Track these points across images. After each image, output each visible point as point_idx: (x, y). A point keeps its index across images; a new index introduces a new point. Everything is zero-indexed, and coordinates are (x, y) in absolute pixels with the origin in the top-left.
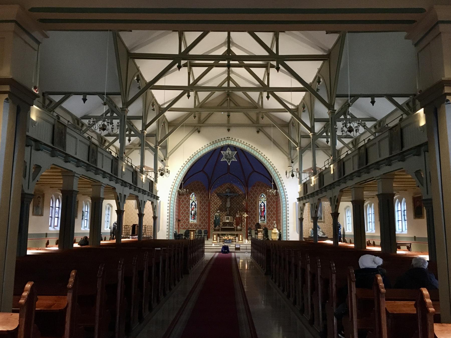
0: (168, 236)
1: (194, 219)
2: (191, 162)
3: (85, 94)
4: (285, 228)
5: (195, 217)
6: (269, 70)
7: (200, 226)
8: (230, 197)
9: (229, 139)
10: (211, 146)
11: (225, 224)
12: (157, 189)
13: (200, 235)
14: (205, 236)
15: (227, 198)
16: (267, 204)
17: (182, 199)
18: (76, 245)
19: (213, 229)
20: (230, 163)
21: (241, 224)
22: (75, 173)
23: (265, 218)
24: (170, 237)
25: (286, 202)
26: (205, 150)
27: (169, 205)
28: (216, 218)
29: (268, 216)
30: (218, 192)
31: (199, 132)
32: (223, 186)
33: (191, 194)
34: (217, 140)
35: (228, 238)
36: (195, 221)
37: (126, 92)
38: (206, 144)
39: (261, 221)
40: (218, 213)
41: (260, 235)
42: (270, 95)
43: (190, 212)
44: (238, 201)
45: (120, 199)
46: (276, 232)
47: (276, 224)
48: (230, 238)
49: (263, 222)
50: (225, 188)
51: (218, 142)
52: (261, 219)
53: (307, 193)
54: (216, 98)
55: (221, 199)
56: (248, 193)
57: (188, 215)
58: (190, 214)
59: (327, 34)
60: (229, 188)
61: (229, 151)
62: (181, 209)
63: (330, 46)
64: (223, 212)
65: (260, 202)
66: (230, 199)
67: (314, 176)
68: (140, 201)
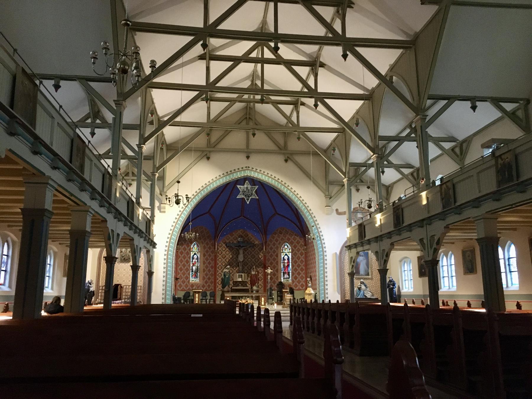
0: (164, 301)
1: (196, 277)
2: (197, 198)
3: (57, 77)
4: (323, 287)
5: (197, 274)
6: (317, 70)
7: (203, 286)
8: (243, 248)
9: (248, 170)
10: (224, 178)
11: (236, 283)
12: (154, 233)
13: (205, 298)
14: (211, 300)
15: (239, 249)
16: (292, 256)
17: (180, 251)
18: (43, 313)
19: (221, 290)
20: (249, 200)
21: (258, 284)
22: (49, 178)
23: (289, 275)
24: (167, 301)
25: (323, 253)
26: (213, 185)
27: (166, 257)
28: (225, 275)
29: (294, 272)
30: (227, 241)
31: (208, 158)
32: (233, 233)
33: (192, 243)
34: (236, 168)
35: (247, 302)
36: (197, 280)
37: (123, 80)
38: (221, 174)
39: (284, 279)
40: (228, 269)
41: (289, 297)
42: (319, 103)
43: (191, 268)
44: (253, 253)
45: (111, 240)
46: (310, 292)
47: (310, 282)
48: (249, 301)
49: (287, 280)
50: (237, 237)
51: (234, 173)
52: (284, 276)
53: (365, 237)
54: (232, 115)
55: (231, 251)
56: (266, 242)
57: (188, 272)
58: (191, 271)
59: (423, 5)
60: (242, 237)
61: (247, 185)
62: (180, 263)
63: (418, 26)
64: (233, 267)
65: (282, 254)
66: (243, 252)
67: (380, 213)
68: (136, 247)
